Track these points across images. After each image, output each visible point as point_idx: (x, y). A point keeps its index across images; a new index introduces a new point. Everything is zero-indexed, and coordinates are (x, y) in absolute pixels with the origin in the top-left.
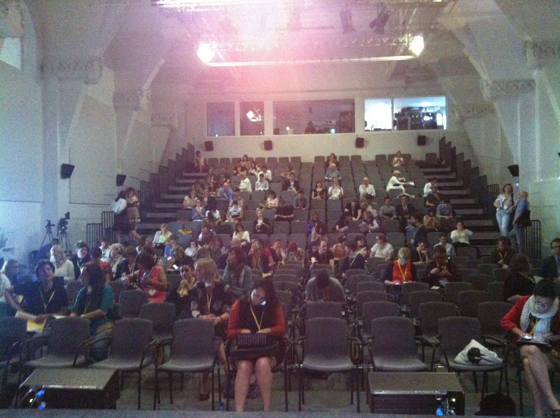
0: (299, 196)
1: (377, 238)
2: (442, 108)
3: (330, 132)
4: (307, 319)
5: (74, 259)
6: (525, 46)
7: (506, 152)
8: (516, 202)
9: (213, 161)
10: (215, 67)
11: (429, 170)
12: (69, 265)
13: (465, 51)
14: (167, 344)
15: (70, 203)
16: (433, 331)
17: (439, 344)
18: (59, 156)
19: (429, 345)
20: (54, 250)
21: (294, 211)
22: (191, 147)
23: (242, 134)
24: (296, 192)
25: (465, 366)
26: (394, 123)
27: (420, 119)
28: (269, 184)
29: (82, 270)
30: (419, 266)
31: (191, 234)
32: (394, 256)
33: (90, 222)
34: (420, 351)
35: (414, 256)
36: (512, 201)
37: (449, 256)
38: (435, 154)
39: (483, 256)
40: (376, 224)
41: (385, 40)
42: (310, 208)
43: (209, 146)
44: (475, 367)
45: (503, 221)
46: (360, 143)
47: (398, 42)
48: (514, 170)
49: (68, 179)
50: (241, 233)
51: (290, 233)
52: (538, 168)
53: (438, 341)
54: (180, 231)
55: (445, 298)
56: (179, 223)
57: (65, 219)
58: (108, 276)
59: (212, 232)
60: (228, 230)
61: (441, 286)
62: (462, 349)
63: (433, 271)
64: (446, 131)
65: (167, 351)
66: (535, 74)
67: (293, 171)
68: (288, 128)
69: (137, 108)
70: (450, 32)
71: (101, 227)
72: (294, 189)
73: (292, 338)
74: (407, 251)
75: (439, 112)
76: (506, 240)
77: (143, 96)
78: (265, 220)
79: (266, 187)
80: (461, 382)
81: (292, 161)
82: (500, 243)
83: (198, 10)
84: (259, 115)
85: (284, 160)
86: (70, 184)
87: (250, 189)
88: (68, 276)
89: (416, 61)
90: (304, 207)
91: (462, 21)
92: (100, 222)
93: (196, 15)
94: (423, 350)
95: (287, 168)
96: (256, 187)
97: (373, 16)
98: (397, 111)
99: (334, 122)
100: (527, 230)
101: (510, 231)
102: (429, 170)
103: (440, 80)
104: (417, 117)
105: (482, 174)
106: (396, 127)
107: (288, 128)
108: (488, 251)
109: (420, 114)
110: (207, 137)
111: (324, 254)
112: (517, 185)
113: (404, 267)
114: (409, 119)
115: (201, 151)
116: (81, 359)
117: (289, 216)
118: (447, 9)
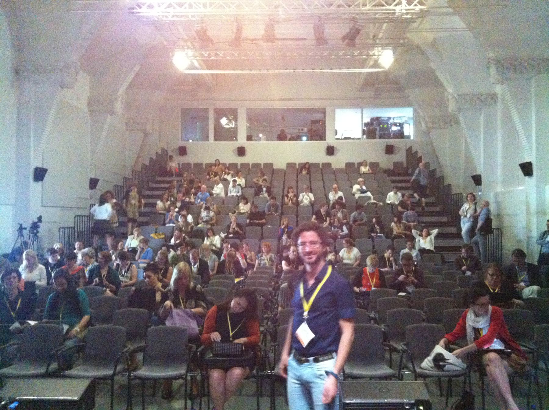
0: (271, 202)
1: (344, 242)
2: (409, 118)
3: (301, 140)
4: (279, 326)
5: (46, 264)
6: (489, 62)
7: (469, 159)
8: (478, 210)
9: (186, 166)
10: (189, 74)
11: (398, 178)
12: (41, 269)
13: (432, 65)
14: (140, 351)
15: (42, 206)
16: (401, 336)
17: (407, 350)
18: (32, 160)
19: (395, 350)
20: (27, 255)
21: (266, 217)
22: (164, 151)
23: (216, 140)
24: (268, 198)
25: (432, 372)
26: (364, 132)
27: (388, 129)
28: (242, 190)
29: (53, 275)
30: (387, 272)
31: (163, 238)
32: (363, 259)
33: (61, 225)
34: (387, 356)
35: (381, 262)
36: (475, 210)
37: (416, 261)
38: (402, 163)
39: (449, 262)
40: (345, 230)
41: (356, 52)
42: (282, 214)
43: (183, 151)
44: (440, 373)
45: (465, 226)
46: (330, 151)
47: (368, 55)
48: (477, 180)
49: (40, 183)
50: (211, 238)
51: (262, 238)
52: (500, 179)
53: (405, 348)
54: (152, 235)
55: (412, 305)
56: (152, 227)
57: (38, 222)
58: (81, 280)
59: (184, 237)
60: (201, 235)
61: (408, 293)
62: (428, 355)
63: (401, 278)
64: (413, 141)
65: (140, 357)
66: (498, 89)
67: (265, 177)
68: (261, 135)
69: (112, 112)
70: (418, 47)
71: (73, 230)
72: (266, 195)
73: (264, 344)
74: (375, 258)
75: (406, 122)
76: (469, 248)
77: (117, 101)
78: (238, 225)
79: (238, 193)
80: (427, 386)
81: (264, 167)
82: (463, 251)
83: (174, 19)
84: (232, 121)
85: (256, 166)
86: (42, 186)
87: (223, 194)
88: (40, 280)
89: (386, 73)
90: (276, 213)
91: (430, 37)
92: (72, 225)
93: (173, 23)
94: (391, 355)
95: (259, 173)
96: (229, 192)
97: (345, 30)
98: (367, 120)
99: (306, 130)
100: (489, 237)
101: (473, 238)
102: (398, 178)
103: (408, 91)
104: (385, 126)
105: (446, 183)
106: (365, 137)
107: (261, 135)
108: (451, 257)
109: (388, 124)
110: (180, 141)
111: (294, 259)
112: (480, 193)
113: (372, 275)
114: (378, 128)
115: (174, 156)
116: (54, 366)
117: (260, 221)
118: (415, 25)
